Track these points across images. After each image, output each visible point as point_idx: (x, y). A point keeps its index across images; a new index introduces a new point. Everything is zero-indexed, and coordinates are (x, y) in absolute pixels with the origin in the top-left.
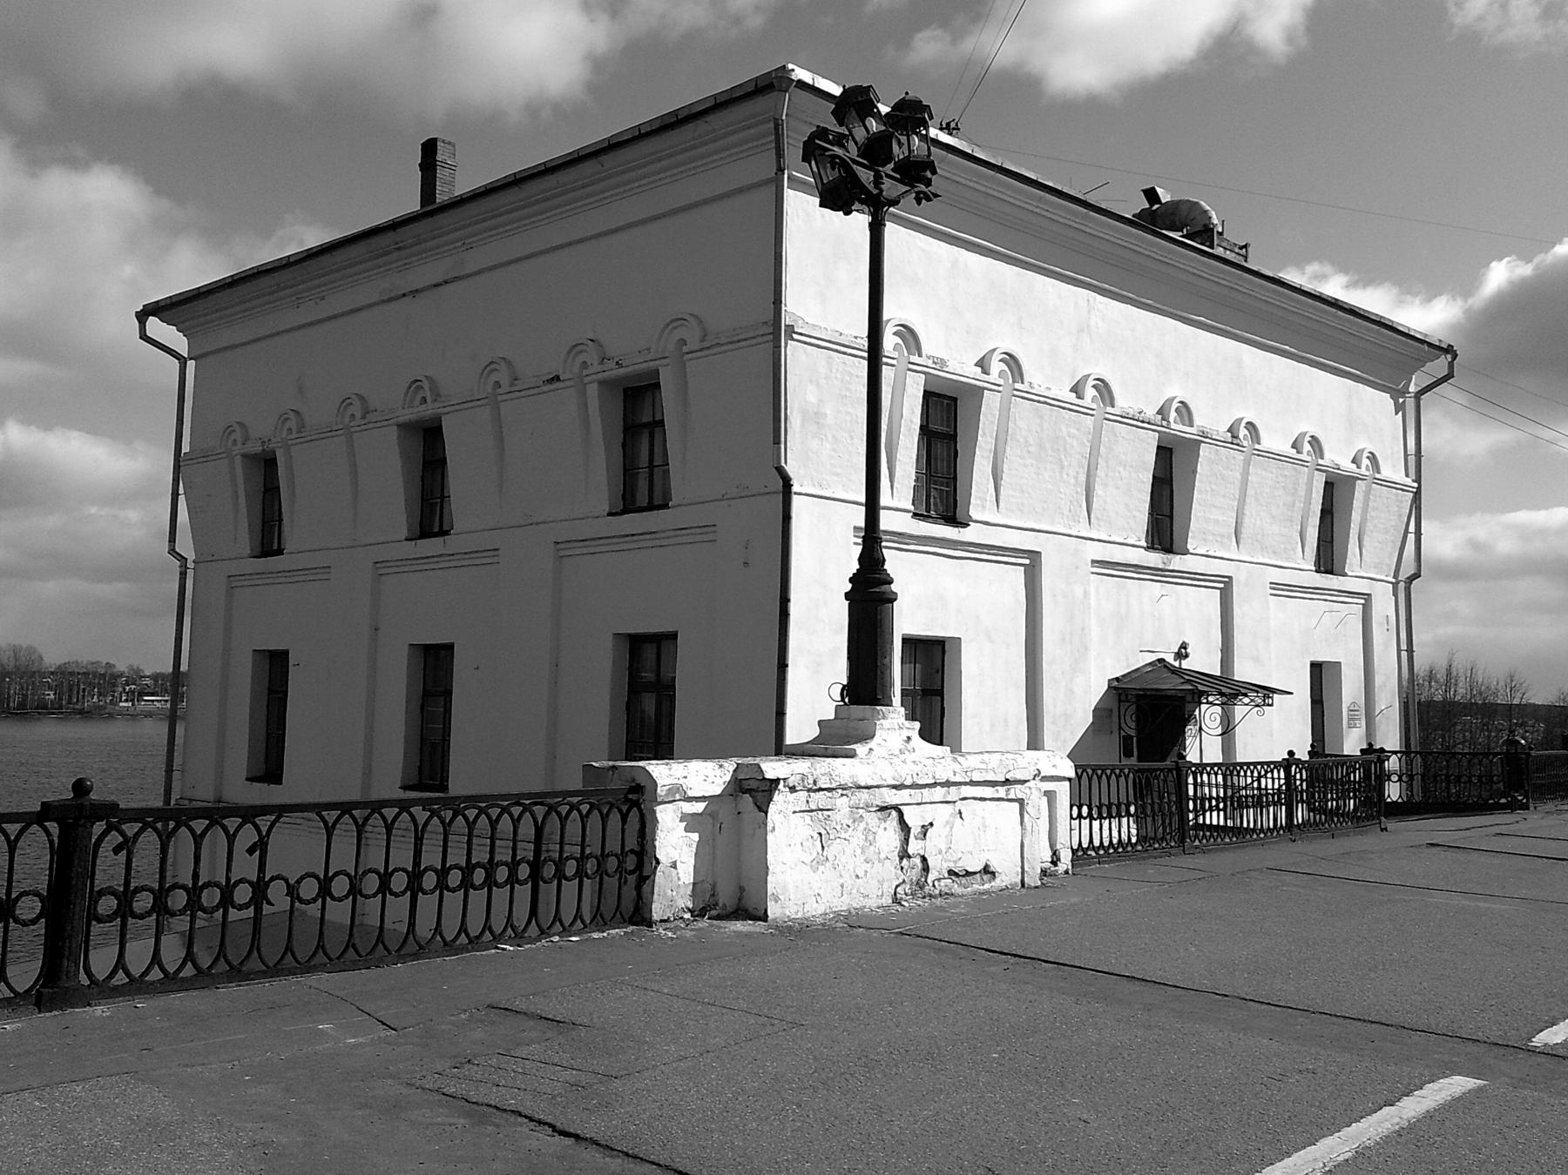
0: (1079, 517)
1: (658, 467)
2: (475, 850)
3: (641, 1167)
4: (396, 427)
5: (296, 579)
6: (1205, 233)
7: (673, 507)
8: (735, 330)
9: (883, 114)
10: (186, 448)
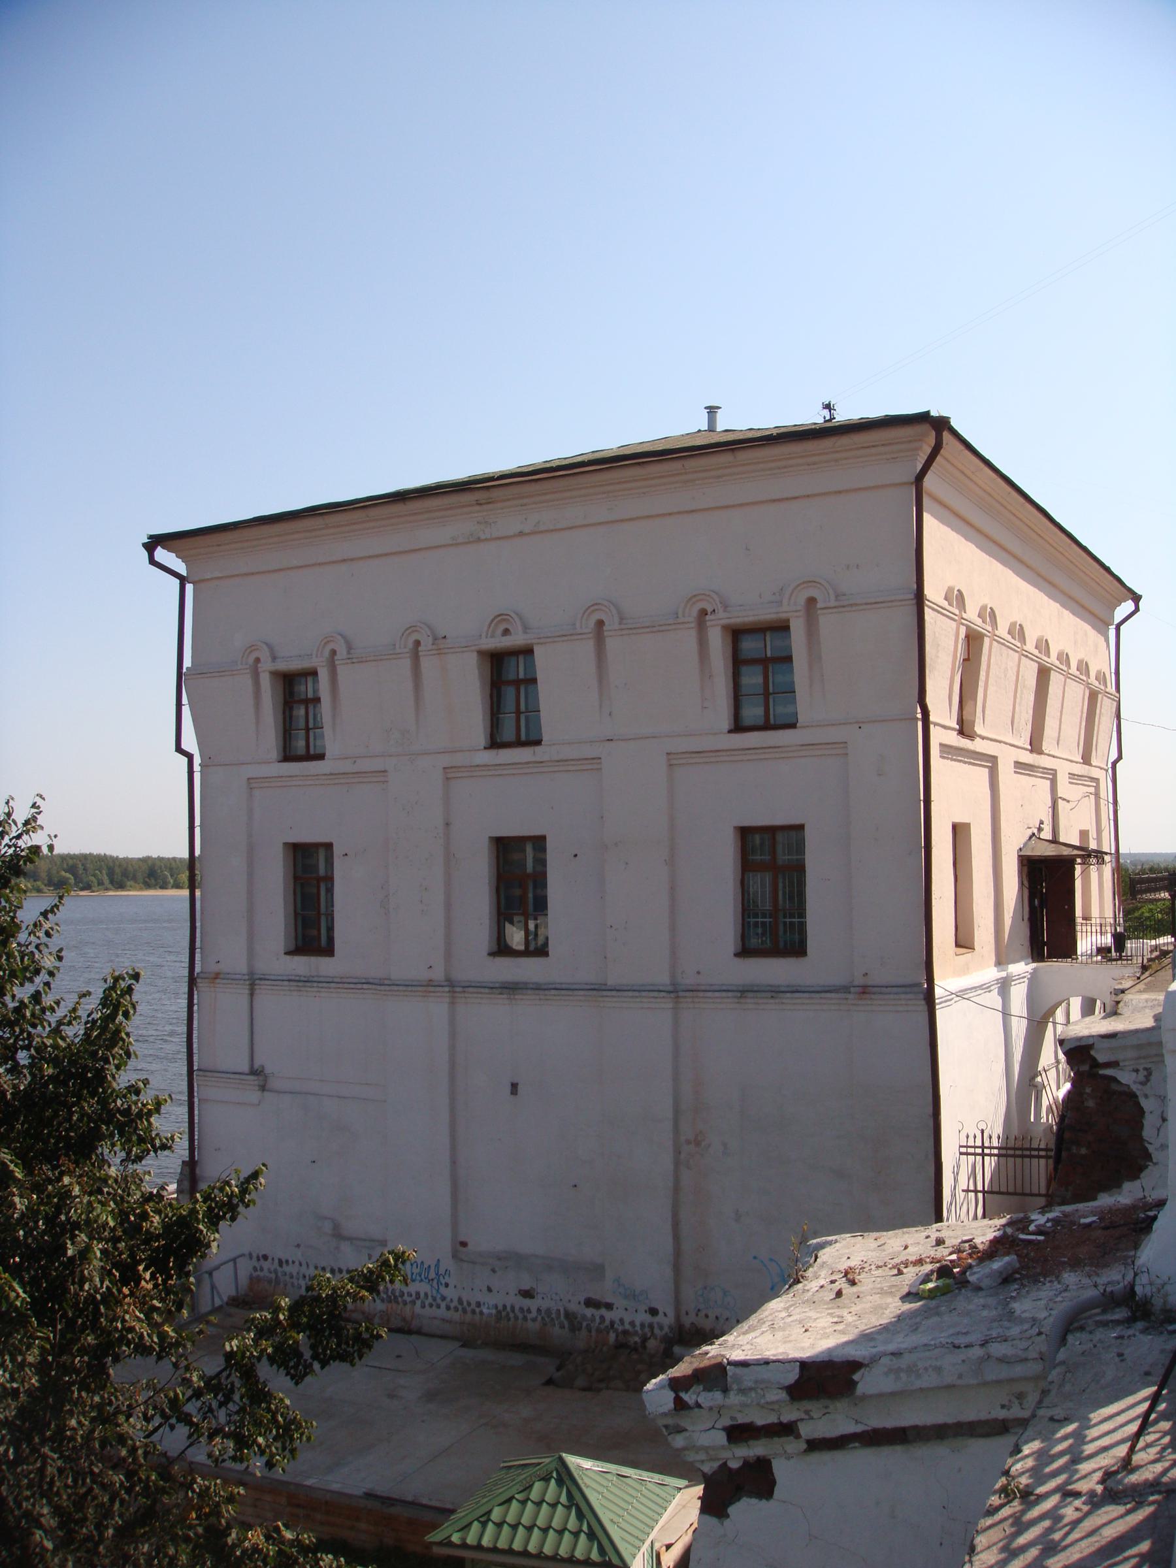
0: (86, 1069)
2: (185, 1122)
3: (729, 1398)
4: (475, 654)
5: (336, 781)
6: (580, 1389)
7: (800, 727)
9: (1154, 1024)
10: (187, 663)
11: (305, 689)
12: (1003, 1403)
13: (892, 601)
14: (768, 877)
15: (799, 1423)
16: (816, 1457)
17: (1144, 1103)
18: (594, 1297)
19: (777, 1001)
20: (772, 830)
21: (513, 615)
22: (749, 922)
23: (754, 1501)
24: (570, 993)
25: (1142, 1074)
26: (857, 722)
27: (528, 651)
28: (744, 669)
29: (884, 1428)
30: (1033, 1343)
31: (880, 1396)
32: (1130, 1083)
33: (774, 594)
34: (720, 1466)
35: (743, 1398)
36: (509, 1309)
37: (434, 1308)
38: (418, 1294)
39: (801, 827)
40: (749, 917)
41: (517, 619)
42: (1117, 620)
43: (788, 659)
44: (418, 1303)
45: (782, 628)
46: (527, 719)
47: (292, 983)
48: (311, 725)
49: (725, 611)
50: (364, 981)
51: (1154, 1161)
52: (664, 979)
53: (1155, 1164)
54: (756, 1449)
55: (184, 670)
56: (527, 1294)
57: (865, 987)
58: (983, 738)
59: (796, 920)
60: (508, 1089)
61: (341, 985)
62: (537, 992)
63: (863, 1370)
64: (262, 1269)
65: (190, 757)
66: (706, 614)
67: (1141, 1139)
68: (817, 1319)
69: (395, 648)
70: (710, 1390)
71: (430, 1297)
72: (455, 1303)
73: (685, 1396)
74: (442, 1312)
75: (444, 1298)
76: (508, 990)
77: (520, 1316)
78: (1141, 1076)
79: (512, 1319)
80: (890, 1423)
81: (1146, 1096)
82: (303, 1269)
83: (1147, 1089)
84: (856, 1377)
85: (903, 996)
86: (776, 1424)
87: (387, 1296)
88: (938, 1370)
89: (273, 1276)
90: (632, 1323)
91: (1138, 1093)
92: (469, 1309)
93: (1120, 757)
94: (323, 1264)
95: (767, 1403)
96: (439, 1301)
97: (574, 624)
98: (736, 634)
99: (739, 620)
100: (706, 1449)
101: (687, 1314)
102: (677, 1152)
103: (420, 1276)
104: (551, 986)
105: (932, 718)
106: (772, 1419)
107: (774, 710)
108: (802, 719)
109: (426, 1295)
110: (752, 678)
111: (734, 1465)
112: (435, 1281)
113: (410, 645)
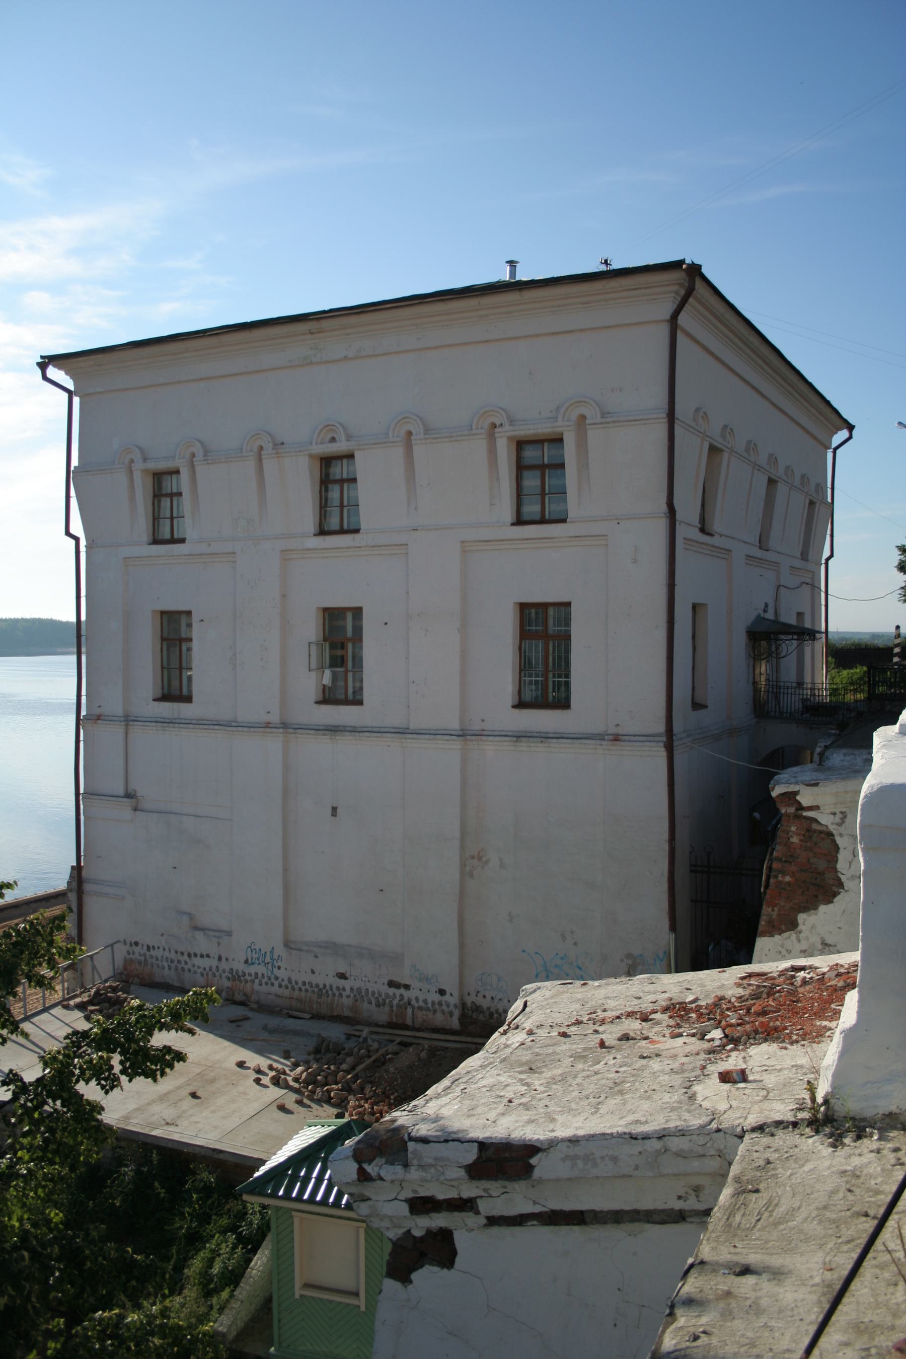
1: (349, 506)
3: (410, 1173)
4: (307, 458)
5: (763, 565)
7: (570, 522)
8: (759, 470)
10: (75, 462)
11: (169, 485)
12: (680, 1194)
13: (648, 419)
14: (541, 644)
15: (479, 1201)
16: (495, 1230)
17: (839, 840)
18: (395, 979)
19: (545, 745)
20: (545, 606)
21: (338, 426)
22: (525, 680)
23: (435, 1269)
24: (379, 735)
25: (839, 816)
26: (617, 519)
27: (351, 456)
28: (526, 474)
29: (561, 1210)
30: (711, 1139)
31: (557, 1180)
32: (829, 824)
33: (551, 411)
34: (405, 1233)
35: (424, 1174)
36: (328, 987)
37: (269, 985)
38: (256, 974)
39: (569, 604)
40: (525, 677)
41: (341, 429)
42: (834, 445)
43: (562, 466)
44: (257, 981)
45: (558, 441)
46: (348, 511)
47: (158, 724)
48: (175, 515)
49: (510, 425)
50: (215, 723)
51: (846, 888)
52: (455, 725)
53: (847, 891)
54: (439, 1221)
55: (72, 468)
56: (342, 976)
57: (618, 735)
58: (721, 535)
59: (563, 679)
60: (330, 811)
61: (197, 726)
62: (353, 733)
63: (540, 1155)
64: (134, 953)
65: (77, 539)
66: (495, 427)
67: (835, 870)
68: (507, 1085)
69: (242, 452)
70: (392, 1164)
71: (266, 977)
72: (286, 982)
73: (369, 1168)
74: (275, 989)
75: (277, 978)
76: (330, 732)
77: (337, 993)
78: (838, 819)
79: (331, 996)
80: (567, 1206)
81: (841, 835)
82: (166, 954)
83: (842, 829)
84: (533, 1161)
85: (647, 744)
86: (456, 1199)
87: (233, 975)
88: (615, 1159)
89: (143, 958)
90: (425, 1001)
91: (834, 832)
92: (297, 987)
93: (832, 556)
94: (181, 949)
95: (446, 1180)
96: (273, 980)
97: (388, 434)
98: (521, 444)
99: (522, 433)
100: (391, 1218)
101: (469, 994)
102: (463, 865)
103: (258, 960)
104: (364, 729)
105: (678, 517)
106: (452, 1194)
107: (549, 507)
108: (571, 515)
109: (263, 975)
110: (531, 481)
111: (418, 1233)
112: (270, 964)
113: (255, 450)
